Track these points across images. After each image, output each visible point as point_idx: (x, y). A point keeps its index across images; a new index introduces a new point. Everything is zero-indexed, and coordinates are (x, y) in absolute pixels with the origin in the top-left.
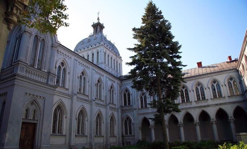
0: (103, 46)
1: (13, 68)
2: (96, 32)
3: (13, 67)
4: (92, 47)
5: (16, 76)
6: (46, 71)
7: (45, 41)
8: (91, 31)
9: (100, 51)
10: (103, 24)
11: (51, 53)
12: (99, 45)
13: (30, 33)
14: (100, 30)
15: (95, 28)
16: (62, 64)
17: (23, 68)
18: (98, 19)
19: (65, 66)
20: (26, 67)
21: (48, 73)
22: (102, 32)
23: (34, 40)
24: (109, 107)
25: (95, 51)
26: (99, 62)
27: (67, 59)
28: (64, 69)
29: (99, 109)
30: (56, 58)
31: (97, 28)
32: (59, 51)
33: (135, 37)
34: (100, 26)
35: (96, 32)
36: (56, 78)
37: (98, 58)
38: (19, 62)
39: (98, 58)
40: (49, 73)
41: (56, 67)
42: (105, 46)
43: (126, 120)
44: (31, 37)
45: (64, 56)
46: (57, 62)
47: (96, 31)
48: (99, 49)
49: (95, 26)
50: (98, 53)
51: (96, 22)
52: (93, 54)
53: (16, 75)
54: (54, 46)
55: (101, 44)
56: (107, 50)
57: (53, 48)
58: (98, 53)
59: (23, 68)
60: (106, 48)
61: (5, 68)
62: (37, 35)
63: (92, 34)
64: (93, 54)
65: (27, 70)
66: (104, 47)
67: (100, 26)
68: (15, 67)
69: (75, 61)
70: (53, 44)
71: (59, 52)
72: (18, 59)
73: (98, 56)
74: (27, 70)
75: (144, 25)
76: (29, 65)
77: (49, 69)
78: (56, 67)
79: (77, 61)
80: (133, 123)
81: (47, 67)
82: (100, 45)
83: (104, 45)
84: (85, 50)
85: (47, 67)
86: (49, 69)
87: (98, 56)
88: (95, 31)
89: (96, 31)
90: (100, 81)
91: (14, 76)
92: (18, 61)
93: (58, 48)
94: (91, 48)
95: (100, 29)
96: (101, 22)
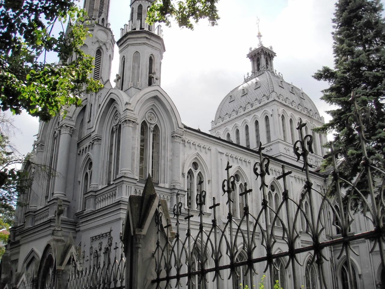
0: (275, 102)
1: (115, 188)
2: (258, 69)
3: (114, 186)
4: (254, 108)
5: (122, 205)
6: (167, 186)
7: (160, 131)
8: (248, 66)
9: (272, 115)
10: (271, 48)
11: (173, 150)
12: (267, 101)
13: (133, 122)
14: (267, 64)
15: (256, 59)
16: (195, 165)
17: (130, 187)
18: (259, 36)
19: (200, 169)
20: (134, 184)
21: (171, 189)
22: (271, 65)
23: (141, 131)
24: (300, 242)
25: (260, 116)
26: (272, 139)
27: (202, 155)
28: (200, 174)
29: (279, 248)
30: (181, 156)
31: (258, 60)
32: (186, 141)
33: (332, 104)
34: (265, 54)
35: (258, 69)
36: (186, 196)
37: (268, 132)
38: (123, 179)
39: (268, 132)
40: (172, 189)
41: (183, 174)
42: (279, 101)
43: (343, 268)
44: (136, 129)
45: (196, 149)
46: (184, 164)
47: (258, 65)
48: (269, 110)
49: (255, 55)
50: (267, 118)
51: (255, 46)
52: (257, 123)
53: (121, 202)
54: (176, 136)
55: (272, 99)
56: (286, 109)
57: (175, 140)
58: (267, 118)
59: (130, 187)
60: (285, 105)
61: (100, 188)
62: (144, 120)
63: (250, 75)
64: (257, 123)
65: (136, 189)
66: (279, 104)
67: (265, 54)
68: (117, 188)
69: (219, 154)
70: (174, 132)
71: (186, 144)
72: (119, 172)
73: (268, 126)
74: (136, 189)
75: (380, 14)
76: (138, 180)
77: (172, 181)
78: (183, 174)
79: (223, 154)
80: (360, 273)
81: (168, 179)
82: (270, 100)
83: (277, 99)
84: (239, 114)
85: (168, 179)
86: (172, 181)
87: (268, 126)
88: (256, 68)
89: (258, 65)
90: (275, 186)
91: (118, 204)
92: (121, 177)
93: (184, 137)
94: (251, 109)
95: (267, 61)
96: (266, 45)
